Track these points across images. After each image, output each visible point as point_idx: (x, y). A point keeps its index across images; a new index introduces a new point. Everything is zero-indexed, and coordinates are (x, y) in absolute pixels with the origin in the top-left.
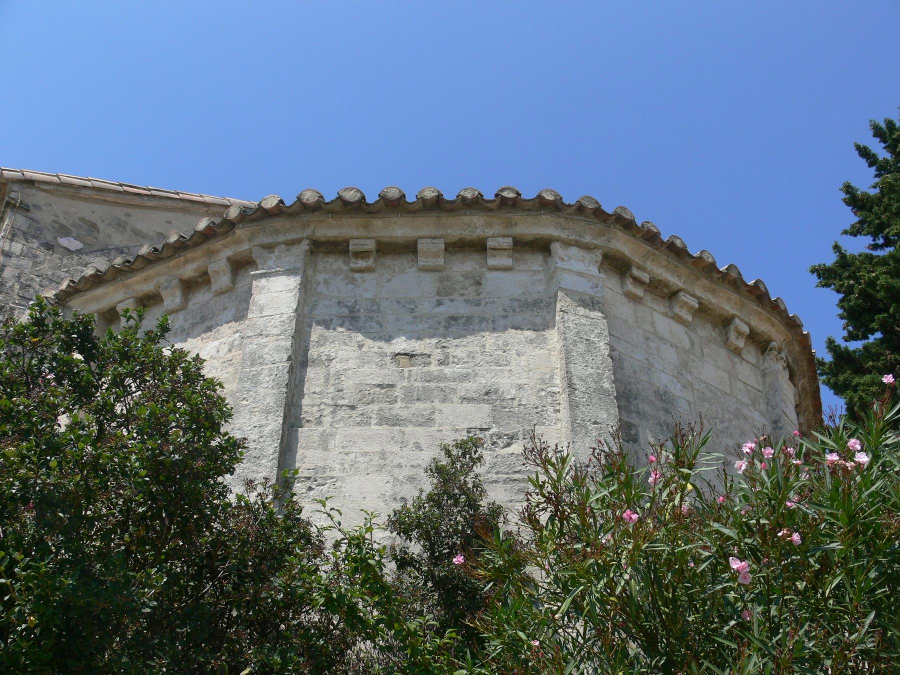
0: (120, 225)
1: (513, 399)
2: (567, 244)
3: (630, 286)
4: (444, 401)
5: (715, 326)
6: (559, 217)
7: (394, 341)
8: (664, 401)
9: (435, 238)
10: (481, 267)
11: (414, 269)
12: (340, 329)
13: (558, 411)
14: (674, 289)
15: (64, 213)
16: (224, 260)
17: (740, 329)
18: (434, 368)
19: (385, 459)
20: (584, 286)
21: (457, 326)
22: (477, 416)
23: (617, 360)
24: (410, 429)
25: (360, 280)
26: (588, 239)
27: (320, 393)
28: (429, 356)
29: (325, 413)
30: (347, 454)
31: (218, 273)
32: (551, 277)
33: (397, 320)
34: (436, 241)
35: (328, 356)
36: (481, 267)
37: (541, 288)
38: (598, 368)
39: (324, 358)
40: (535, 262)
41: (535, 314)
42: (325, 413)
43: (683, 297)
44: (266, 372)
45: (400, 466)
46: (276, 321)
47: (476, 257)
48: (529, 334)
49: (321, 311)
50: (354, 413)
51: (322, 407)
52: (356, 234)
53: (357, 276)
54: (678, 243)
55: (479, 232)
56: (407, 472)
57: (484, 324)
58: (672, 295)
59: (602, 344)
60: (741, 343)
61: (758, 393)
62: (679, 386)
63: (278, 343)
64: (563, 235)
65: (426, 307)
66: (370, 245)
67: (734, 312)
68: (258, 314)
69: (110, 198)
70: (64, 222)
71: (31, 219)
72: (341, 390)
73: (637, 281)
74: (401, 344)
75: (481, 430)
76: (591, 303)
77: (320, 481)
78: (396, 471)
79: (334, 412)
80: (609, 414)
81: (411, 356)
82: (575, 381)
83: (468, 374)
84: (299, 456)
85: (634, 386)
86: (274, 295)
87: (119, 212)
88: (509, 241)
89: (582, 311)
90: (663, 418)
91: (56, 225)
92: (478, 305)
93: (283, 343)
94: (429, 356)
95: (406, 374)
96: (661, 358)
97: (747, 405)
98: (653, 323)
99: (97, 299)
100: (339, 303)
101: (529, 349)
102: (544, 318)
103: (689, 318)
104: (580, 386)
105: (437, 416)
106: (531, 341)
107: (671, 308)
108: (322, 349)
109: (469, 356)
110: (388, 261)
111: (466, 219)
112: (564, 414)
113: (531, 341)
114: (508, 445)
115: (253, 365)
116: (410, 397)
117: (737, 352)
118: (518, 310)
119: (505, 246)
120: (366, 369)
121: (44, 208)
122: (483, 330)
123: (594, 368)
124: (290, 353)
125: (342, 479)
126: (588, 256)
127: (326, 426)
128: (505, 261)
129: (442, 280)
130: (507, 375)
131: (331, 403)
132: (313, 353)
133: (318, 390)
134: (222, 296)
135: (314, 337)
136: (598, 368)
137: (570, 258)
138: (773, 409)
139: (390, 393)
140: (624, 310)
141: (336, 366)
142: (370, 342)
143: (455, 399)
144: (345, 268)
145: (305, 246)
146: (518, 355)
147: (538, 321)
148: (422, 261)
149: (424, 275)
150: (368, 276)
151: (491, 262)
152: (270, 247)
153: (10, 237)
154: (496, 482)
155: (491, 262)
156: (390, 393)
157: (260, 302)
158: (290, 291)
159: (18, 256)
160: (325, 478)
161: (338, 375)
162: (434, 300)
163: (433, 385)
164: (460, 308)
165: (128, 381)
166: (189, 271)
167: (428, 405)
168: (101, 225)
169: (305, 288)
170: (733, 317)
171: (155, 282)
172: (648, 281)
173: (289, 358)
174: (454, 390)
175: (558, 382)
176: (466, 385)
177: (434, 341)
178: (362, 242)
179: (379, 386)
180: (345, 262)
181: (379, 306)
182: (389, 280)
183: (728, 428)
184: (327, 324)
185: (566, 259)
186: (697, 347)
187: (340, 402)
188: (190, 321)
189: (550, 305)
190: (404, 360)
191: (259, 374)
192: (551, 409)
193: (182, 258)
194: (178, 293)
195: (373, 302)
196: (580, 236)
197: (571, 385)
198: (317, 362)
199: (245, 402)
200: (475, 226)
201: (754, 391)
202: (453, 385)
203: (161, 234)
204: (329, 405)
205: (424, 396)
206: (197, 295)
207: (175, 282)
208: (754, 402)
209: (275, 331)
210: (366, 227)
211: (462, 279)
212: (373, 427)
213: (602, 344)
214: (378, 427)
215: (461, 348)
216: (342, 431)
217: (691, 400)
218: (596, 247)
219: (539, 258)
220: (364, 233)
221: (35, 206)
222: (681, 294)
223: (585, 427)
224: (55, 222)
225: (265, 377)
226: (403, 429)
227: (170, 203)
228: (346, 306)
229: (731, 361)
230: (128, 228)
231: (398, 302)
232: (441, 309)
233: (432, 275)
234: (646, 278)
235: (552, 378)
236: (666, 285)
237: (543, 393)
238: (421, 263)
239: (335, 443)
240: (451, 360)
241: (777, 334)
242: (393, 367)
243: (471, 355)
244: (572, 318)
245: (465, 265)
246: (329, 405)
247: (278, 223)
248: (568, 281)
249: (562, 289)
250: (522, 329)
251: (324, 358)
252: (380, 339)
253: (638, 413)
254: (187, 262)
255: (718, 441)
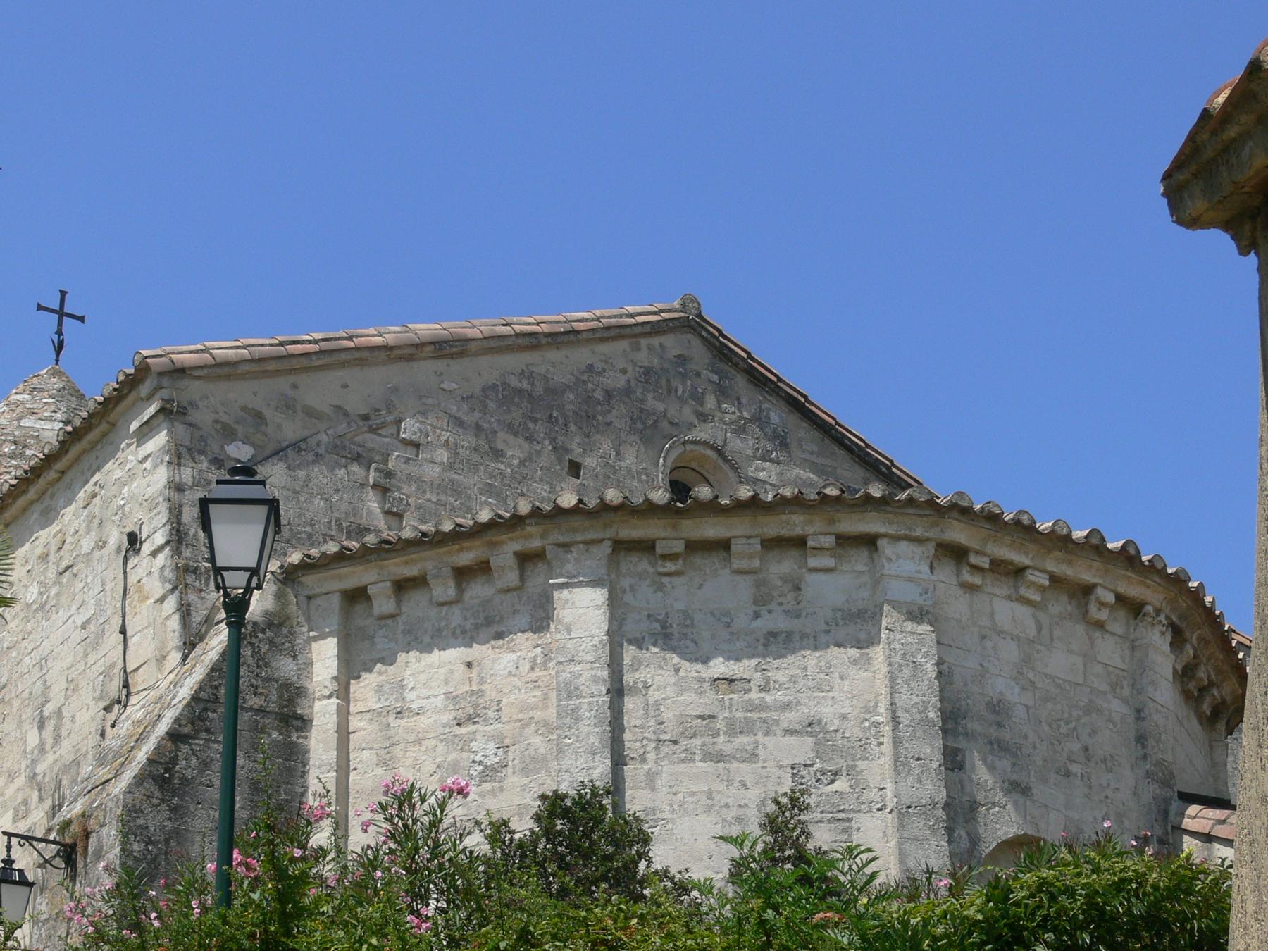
0: (288, 406)
1: (836, 731)
2: (896, 538)
3: (967, 576)
4: (767, 734)
5: (1072, 596)
6: (886, 512)
7: (712, 663)
8: (998, 713)
9: (749, 537)
10: (800, 568)
11: (727, 571)
12: (655, 650)
13: (882, 743)
14: (1020, 566)
15: (223, 405)
16: (511, 555)
17: (1102, 599)
18: (754, 695)
19: (712, 799)
20: (912, 594)
21: (777, 643)
22: (801, 749)
23: (944, 675)
24: (734, 765)
25: (669, 586)
26: (919, 532)
27: (641, 727)
28: (749, 681)
29: (648, 749)
30: (675, 794)
31: (503, 568)
32: (876, 583)
33: (713, 637)
34: (751, 541)
35: (645, 682)
36: (800, 568)
37: (865, 593)
38: (924, 695)
39: (640, 685)
40: (859, 560)
41: (856, 627)
42: (648, 749)
43: (1031, 576)
44: (585, 706)
45: (727, 806)
46: (588, 645)
47: (794, 553)
48: (853, 652)
49: (630, 628)
50: (678, 748)
51: (645, 742)
52: (663, 535)
53: (665, 580)
54: (1025, 519)
55: (798, 531)
56: (734, 812)
57: (805, 642)
58: (1018, 572)
59: (929, 665)
60: (1103, 615)
61: (1121, 673)
62: (1017, 690)
63: (593, 672)
64: (891, 530)
65: (742, 621)
66: (679, 547)
67: (1096, 580)
68: (564, 635)
69: (271, 366)
70: (225, 418)
71: (190, 425)
72: (662, 723)
73: (976, 568)
74: (719, 667)
75: (805, 765)
76: (917, 615)
77: (651, 823)
78: (724, 811)
79: (657, 748)
80: (933, 748)
81: (730, 681)
82: (899, 713)
83: (790, 702)
84: (627, 798)
85: (963, 703)
86: (581, 611)
87: (283, 384)
88: (832, 539)
89: (909, 626)
90: (995, 734)
91: (218, 427)
92: (798, 616)
93: (599, 673)
94: (749, 681)
95: (727, 704)
96: (998, 659)
97: (1105, 693)
98: (992, 615)
99: (340, 578)
100: (649, 616)
101: (853, 672)
102: (869, 633)
103: (1037, 597)
104: (904, 718)
105: (760, 751)
106: (855, 662)
107: (1016, 588)
108: (637, 675)
109: (790, 681)
110: (698, 560)
111: (784, 517)
112: (887, 748)
113: (855, 662)
114: (832, 782)
115: (570, 697)
116: (734, 729)
117: (1100, 625)
118: (841, 623)
119: (827, 545)
120: (686, 698)
121: (200, 404)
122: (800, 649)
123: (922, 696)
124: (608, 685)
125: (672, 821)
126: (918, 550)
127: (651, 764)
128: (826, 561)
129: (758, 585)
130: (830, 703)
131: (653, 737)
132: (628, 678)
133: (638, 723)
134: (509, 595)
135: (627, 661)
136: (924, 695)
137: (898, 557)
138: (1139, 693)
139: (712, 725)
140: (958, 606)
141: (654, 695)
142: (686, 664)
143: (778, 732)
144: (651, 570)
145: (606, 548)
146: (842, 679)
147: (863, 636)
148: (736, 564)
149: (738, 578)
150: (677, 581)
151: (812, 562)
152: (566, 546)
153: (176, 461)
154: (821, 821)
155: (812, 562)
156: (712, 725)
157: (566, 620)
158: (598, 607)
159: (191, 488)
160: (656, 821)
161: (657, 705)
162: (750, 611)
163: (754, 715)
164: (780, 623)
165: (610, 849)
166: (466, 558)
167: (750, 739)
168: (267, 413)
169: (614, 604)
170: (1095, 586)
171: (419, 566)
172: (987, 566)
173: (608, 691)
174: (776, 722)
175: (882, 710)
176: (789, 715)
177: (754, 662)
178: (670, 543)
179: (700, 717)
180: (650, 563)
181: (692, 620)
182: (701, 586)
183: (1075, 729)
184: (639, 643)
185: (894, 558)
186: (1045, 632)
187: (663, 737)
188: (472, 621)
189: (876, 616)
190: (723, 686)
191: (578, 708)
192: (875, 742)
193: (457, 547)
194: (452, 583)
195: (686, 614)
196: (910, 529)
197: (895, 720)
198: (634, 690)
199: (567, 741)
200: (795, 524)
201: (1117, 672)
202: (775, 715)
203: (338, 407)
204: (651, 740)
205: (746, 728)
206: (472, 584)
207: (447, 571)
208: (1114, 686)
209: (588, 658)
210: (674, 527)
211: (779, 583)
212: (698, 764)
213: (929, 665)
214: (702, 764)
215: (784, 669)
216: (667, 769)
217: (1031, 703)
218: (928, 539)
219: (865, 553)
220: (674, 534)
221: (190, 403)
222: (1028, 572)
223: (908, 765)
224: (216, 421)
225: (584, 713)
226: (728, 765)
227: (343, 356)
228: (657, 621)
229: (1090, 638)
230: (299, 408)
231: (713, 614)
232: (758, 623)
233: (746, 577)
234: (985, 563)
235: (876, 706)
236: (1011, 563)
237: (867, 724)
238: (735, 566)
239: (662, 782)
240: (772, 685)
241: (1151, 595)
242: (712, 695)
243: (793, 679)
244: (898, 637)
245: (782, 566)
246: (651, 740)
247: (576, 521)
248: (897, 590)
249: (889, 602)
250: (845, 647)
251: (640, 685)
252: (696, 660)
253: (966, 734)
254: (462, 549)
255: (1059, 749)
